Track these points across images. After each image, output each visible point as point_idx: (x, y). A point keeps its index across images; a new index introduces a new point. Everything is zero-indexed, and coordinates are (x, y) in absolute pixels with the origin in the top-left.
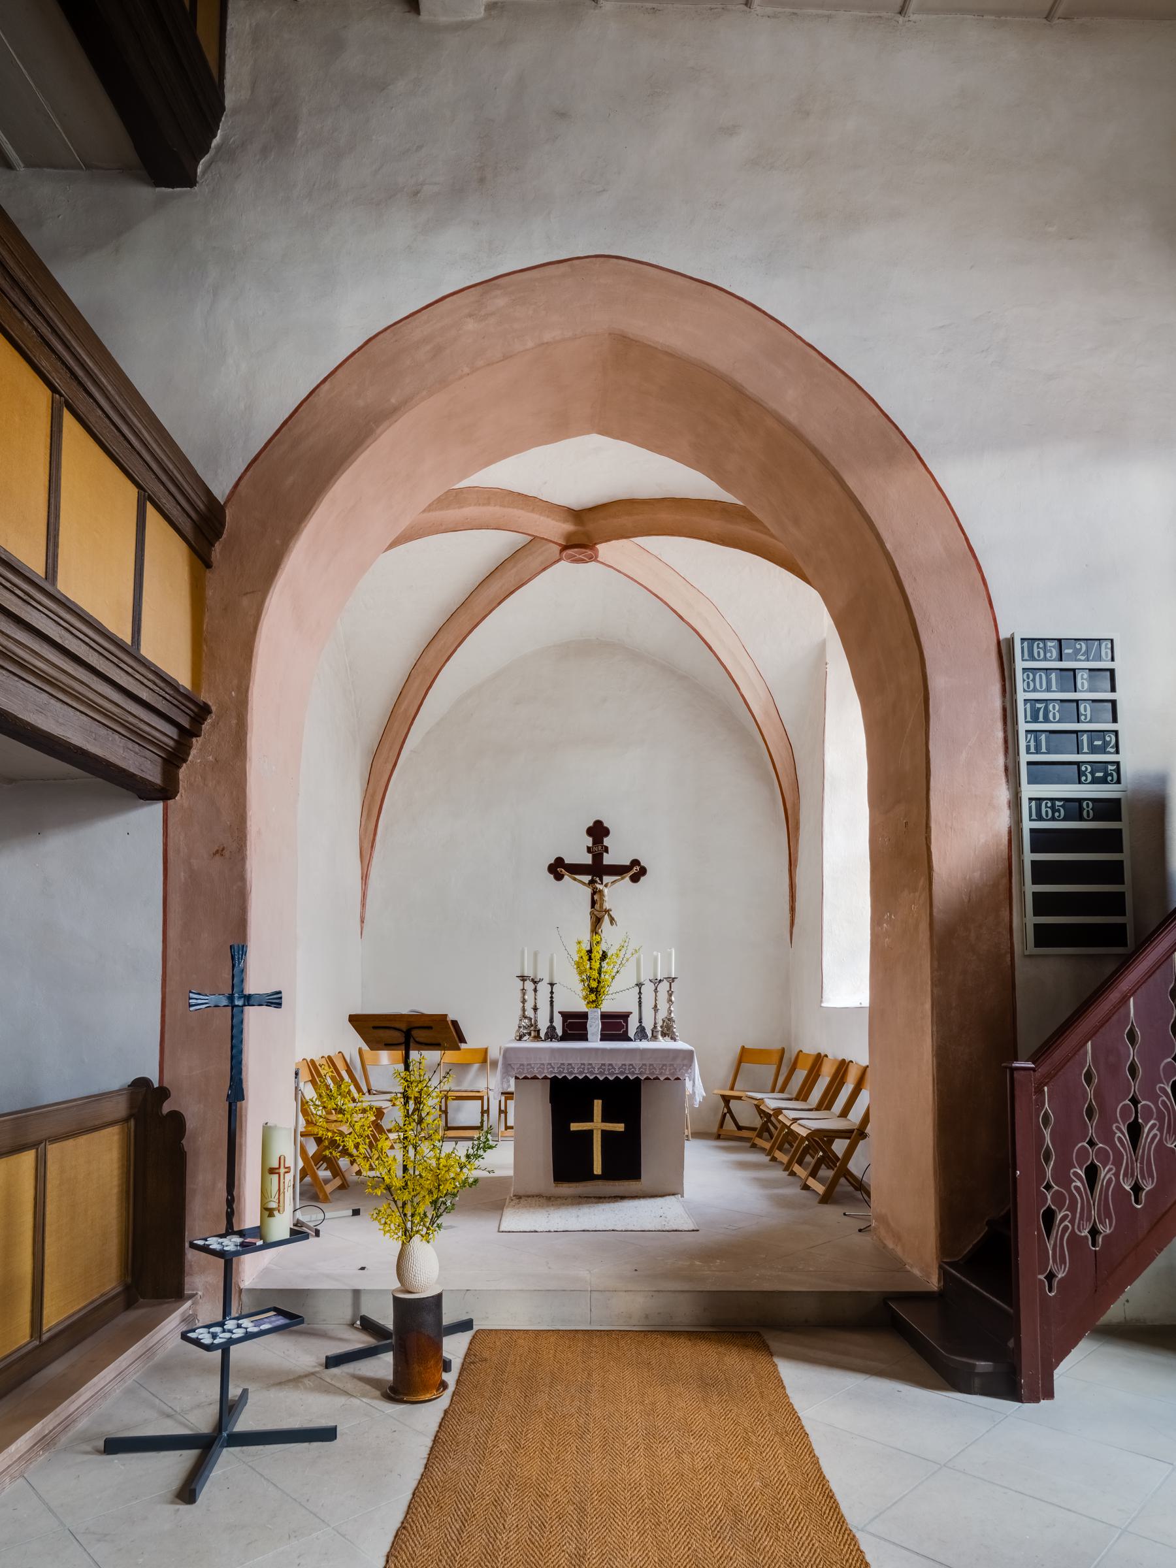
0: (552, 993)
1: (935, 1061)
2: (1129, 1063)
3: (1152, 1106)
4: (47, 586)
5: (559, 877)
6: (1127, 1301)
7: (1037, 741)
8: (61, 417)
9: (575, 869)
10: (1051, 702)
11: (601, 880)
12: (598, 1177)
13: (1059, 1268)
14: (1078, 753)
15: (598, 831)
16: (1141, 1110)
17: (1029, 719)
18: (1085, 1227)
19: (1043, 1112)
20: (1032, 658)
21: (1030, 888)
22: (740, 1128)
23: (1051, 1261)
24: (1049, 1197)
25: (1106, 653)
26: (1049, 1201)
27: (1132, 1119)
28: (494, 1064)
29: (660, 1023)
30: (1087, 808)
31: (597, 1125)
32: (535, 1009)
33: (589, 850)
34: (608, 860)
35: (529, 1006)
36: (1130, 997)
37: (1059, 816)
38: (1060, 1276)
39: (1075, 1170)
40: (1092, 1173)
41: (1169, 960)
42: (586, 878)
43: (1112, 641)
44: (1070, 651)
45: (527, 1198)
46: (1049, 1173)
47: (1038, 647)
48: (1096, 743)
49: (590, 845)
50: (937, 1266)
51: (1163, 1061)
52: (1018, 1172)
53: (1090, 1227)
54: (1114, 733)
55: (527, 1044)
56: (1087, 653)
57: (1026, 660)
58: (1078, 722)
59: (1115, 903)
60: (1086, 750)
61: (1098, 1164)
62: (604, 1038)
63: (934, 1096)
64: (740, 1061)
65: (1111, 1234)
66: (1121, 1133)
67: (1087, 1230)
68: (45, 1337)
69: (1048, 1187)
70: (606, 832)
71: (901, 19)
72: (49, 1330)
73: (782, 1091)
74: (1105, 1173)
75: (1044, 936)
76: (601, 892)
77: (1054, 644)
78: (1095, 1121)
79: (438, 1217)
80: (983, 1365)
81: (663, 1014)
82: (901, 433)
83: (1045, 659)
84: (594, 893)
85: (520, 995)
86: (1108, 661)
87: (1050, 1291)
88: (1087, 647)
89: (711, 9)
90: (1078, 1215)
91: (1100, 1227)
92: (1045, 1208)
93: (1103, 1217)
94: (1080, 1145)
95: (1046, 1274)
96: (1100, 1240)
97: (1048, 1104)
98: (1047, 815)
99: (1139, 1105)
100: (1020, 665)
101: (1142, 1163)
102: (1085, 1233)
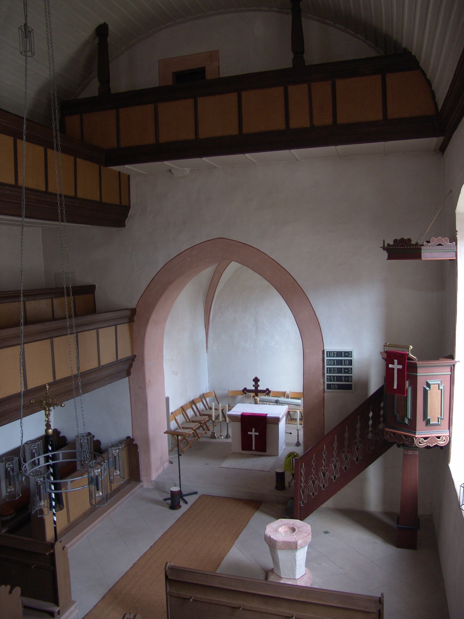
15: (256, 380)
31: (253, 433)
33: (254, 386)
34: (259, 388)
43: (352, 352)
68: (112, 491)
70: (259, 380)
72: (113, 490)
91: (314, 493)
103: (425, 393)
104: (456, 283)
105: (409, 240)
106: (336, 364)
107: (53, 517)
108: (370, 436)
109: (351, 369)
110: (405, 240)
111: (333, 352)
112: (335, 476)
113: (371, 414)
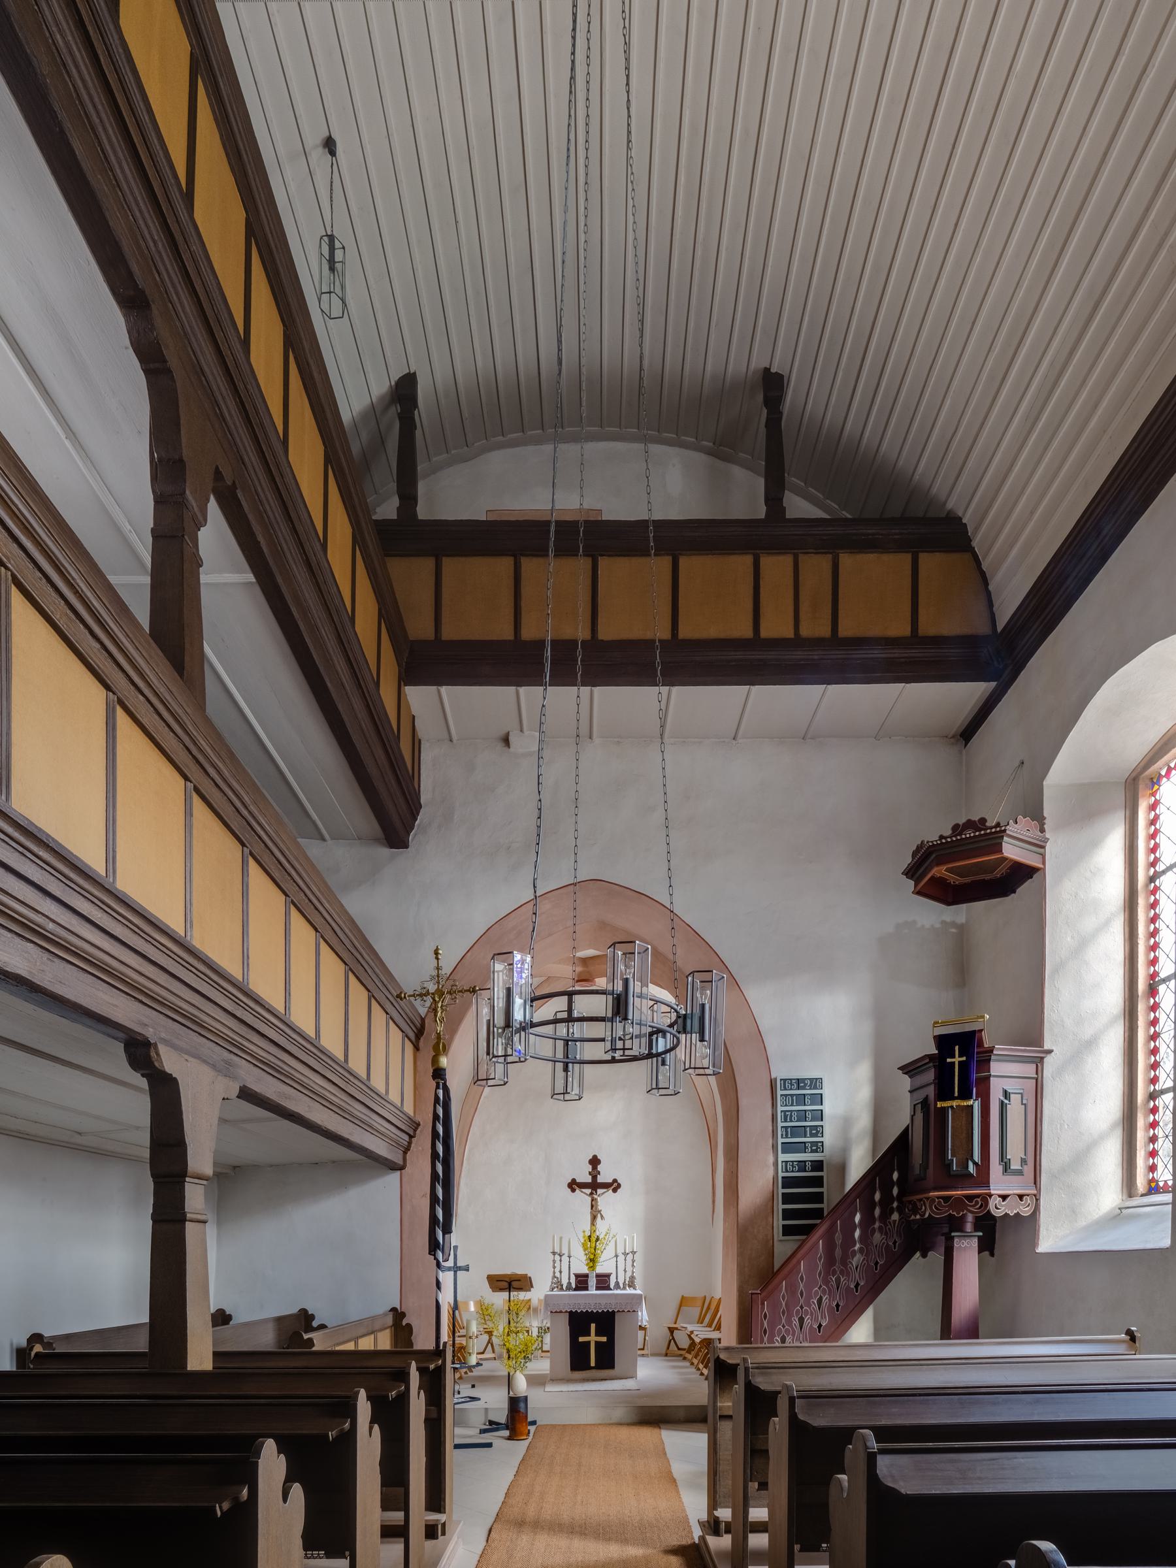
0: (569, 1262)
4: (367, 1083)
5: (573, 1190)
7: (787, 1132)
8: (371, 1001)
9: (582, 1186)
11: (596, 1192)
12: (593, 1368)
15: (595, 1162)
17: (783, 1120)
20: (785, 1089)
21: (782, 1207)
22: (679, 1349)
28: (536, 1310)
29: (628, 1279)
31: (593, 1338)
32: (561, 1272)
34: (600, 1179)
35: (557, 1270)
42: (588, 1191)
43: (821, 1079)
45: (555, 1380)
49: (591, 1170)
55: (556, 1292)
60: (808, 1136)
62: (598, 1288)
64: (680, 1306)
66: (796, 1321)
71: (734, 742)
73: (702, 1323)
75: (787, 1231)
76: (596, 1199)
79: (526, 1363)
81: (629, 1274)
83: (791, 1089)
84: (592, 1200)
85: (552, 1263)
89: (645, 741)
100: (779, 1092)
103: (1003, 1106)
104: (442, 1426)
105: (983, 821)
107: (437, 1273)
108: (895, 1216)
110: (975, 821)
111: (791, 1080)
112: (820, 1323)
113: (895, 1176)
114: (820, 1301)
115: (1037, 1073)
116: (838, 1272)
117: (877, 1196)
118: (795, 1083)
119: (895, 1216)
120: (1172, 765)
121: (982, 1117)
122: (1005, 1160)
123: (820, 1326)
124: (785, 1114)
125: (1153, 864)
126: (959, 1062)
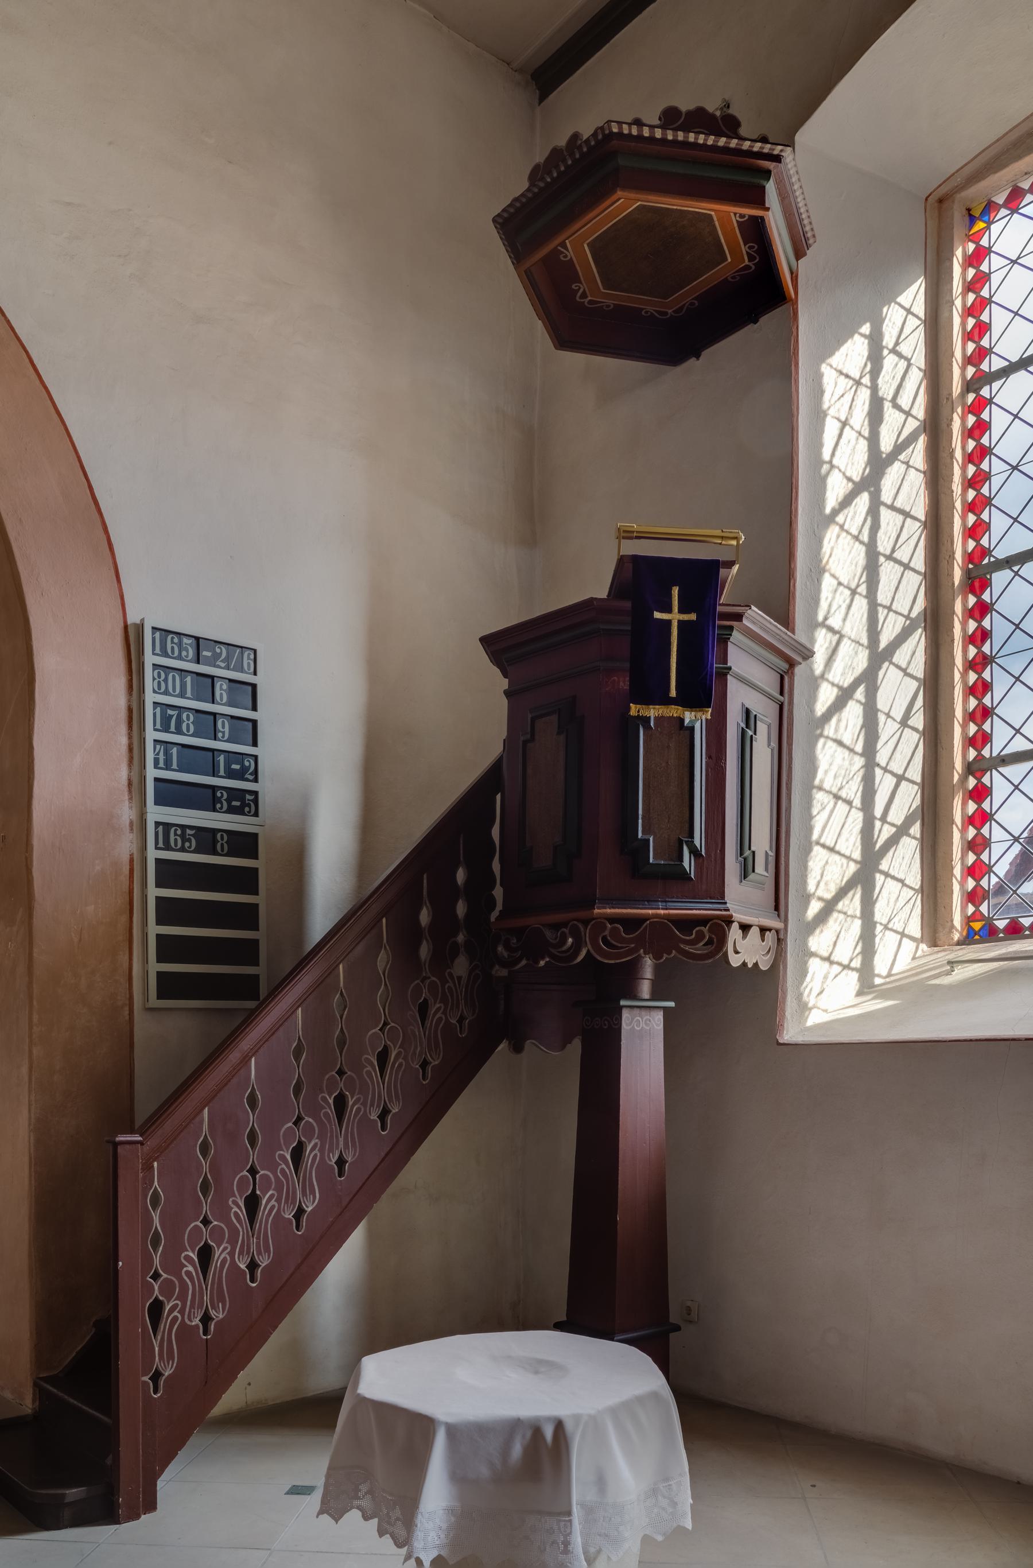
1: (32, 1138)
2: (248, 1130)
3: (271, 1176)
6: (249, 1384)
7: (167, 754)
10: (221, 716)
13: (159, 1364)
14: (214, 776)
16: (259, 1181)
17: (158, 726)
18: (196, 1315)
19: (152, 1191)
21: (154, 929)
23: (157, 1358)
24: (156, 1288)
25: (249, 664)
26: (156, 1292)
27: (250, 1192)
30: (222, 841)
36: (251, 1057)
37: (190, 847)
38: (167, 1374)
39: (186, 1253)
40: (205, 1255)
41: (293, 1016)
43: (255, 651)
44: (209, 654)
46: (157, 1261)
47: (172, 642)
48: (234, 766)
50: (32, 1384)
51: (283, 1126)
52: (120, 1263)
53: (202, 1315)
54: (254, 758)
56: (228, 660)
57: (157, 655)
58: (215, 739)
59: (247, 952)
60: (222, 773)
61: (212, 1244)
63: (30, 1181)
65: (222, 1319)
66: (238, 1208)
67: (199, 1318)
69: (156, 1276)
74: (219, 1252)
77: (191, 641)
78: (210, 1197)
80: (73, 1493)
82: (8, 322)
83: (180, 658)
86: (249, 674)
87: (155, 1392)
88: (228, 653)
90: (189, 1303)
91: (213, 1313)
92: (151, 1301)
93: (216, 1301)
94: (192, 1225)
95: (151, 1374)
96: (212, 1326)
97: (158, 1182)
98: (176, 845)
99: (257, 1176)
100: (150, 659)
101: (258, 1238)
102: (196, 1321)
106: (178, 766)
108: (461, 967)
109: (252, 797)
113: (461, 876)
114: (298, 1154)
115: (782, 693)
116: (342, 1085)
117: (425, 917)
118: (190, 645)
119: (461, 967)
120: (1025, 185)
121: (709, 757)
122: (747, 853)
123: (300, 1212)
124: (163, 714)
125: (982, 353)
126: (679, 621)
